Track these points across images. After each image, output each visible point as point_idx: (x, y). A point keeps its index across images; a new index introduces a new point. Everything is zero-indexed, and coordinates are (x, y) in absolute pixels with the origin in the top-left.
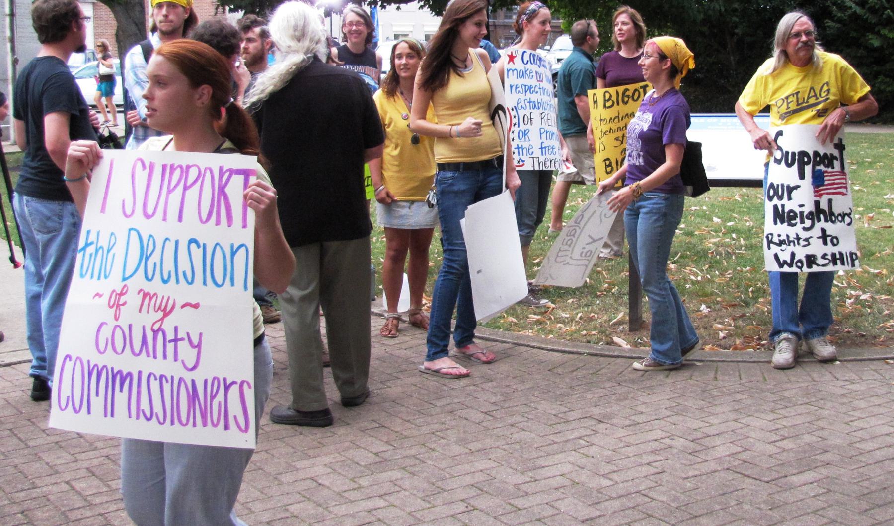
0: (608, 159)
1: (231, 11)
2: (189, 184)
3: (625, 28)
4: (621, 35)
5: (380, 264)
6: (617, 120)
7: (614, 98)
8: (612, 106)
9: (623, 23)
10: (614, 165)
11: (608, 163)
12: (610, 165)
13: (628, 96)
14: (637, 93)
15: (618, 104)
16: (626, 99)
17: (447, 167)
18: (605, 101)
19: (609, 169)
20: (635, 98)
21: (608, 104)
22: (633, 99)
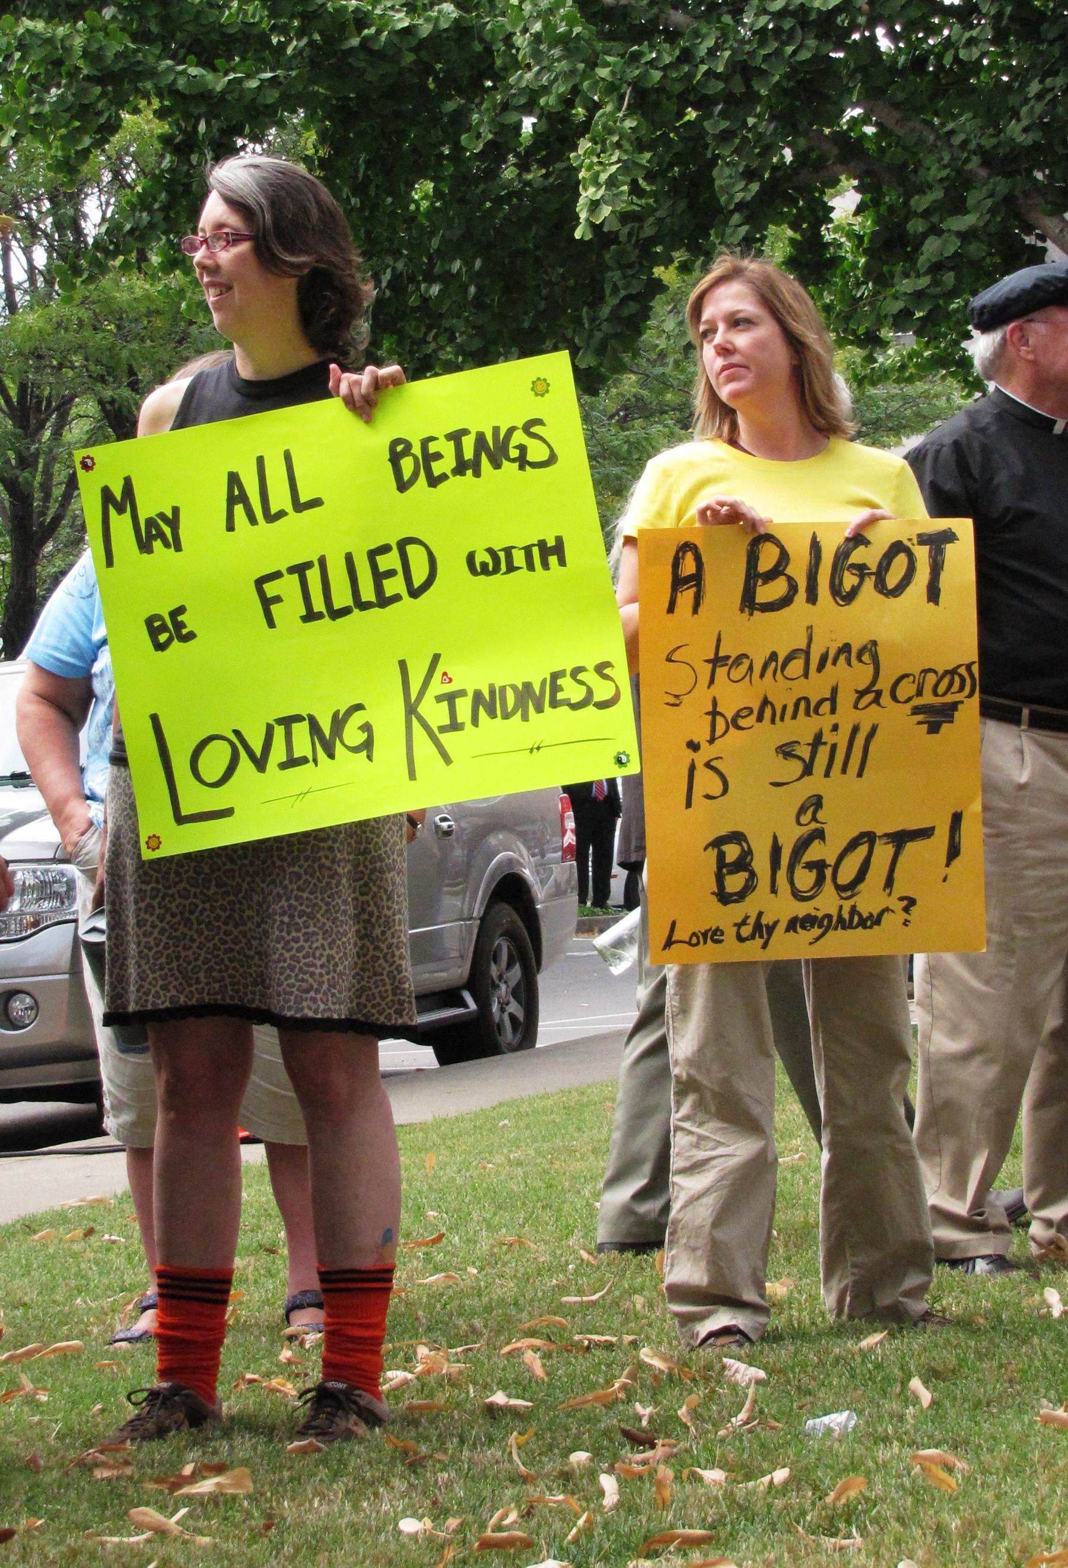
0: (737, 837)
1: (224, 248)
2: (258, 753)
3: (742, 340)
4: (732, 371)
5: (757, 116)
6: (796, 667)
7: (798, 570)
8: (785, 601)
9: (735, 322)
10: (761, 863)
11: (732, 852)
12: (743, 864)
13: (861, 570)
14: (900, 562)
15: (812, 597)
16: (849, 580)
17: (194, 1261)
18: (753, 577)
19: (734, 882)
20: (893, 579)
21: (766, 593)
22: (881, 586)
